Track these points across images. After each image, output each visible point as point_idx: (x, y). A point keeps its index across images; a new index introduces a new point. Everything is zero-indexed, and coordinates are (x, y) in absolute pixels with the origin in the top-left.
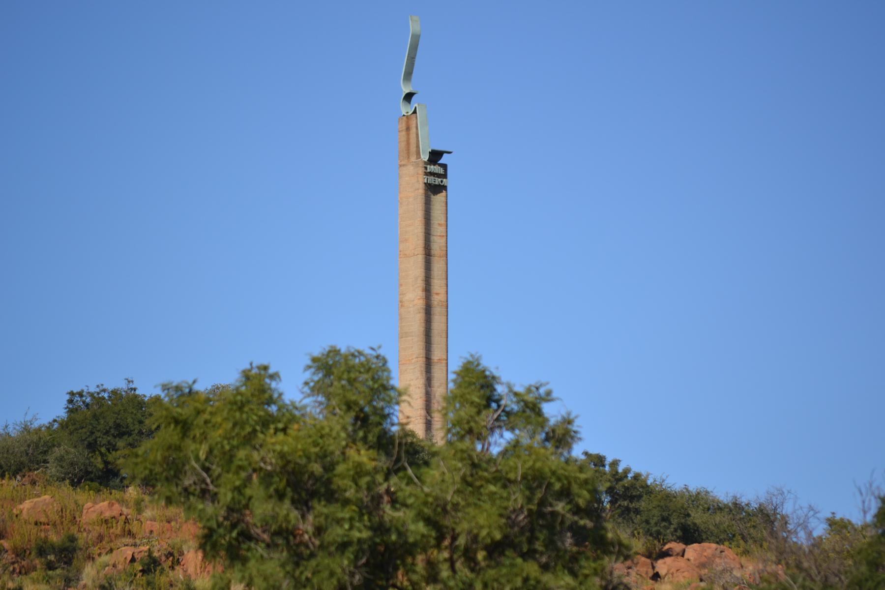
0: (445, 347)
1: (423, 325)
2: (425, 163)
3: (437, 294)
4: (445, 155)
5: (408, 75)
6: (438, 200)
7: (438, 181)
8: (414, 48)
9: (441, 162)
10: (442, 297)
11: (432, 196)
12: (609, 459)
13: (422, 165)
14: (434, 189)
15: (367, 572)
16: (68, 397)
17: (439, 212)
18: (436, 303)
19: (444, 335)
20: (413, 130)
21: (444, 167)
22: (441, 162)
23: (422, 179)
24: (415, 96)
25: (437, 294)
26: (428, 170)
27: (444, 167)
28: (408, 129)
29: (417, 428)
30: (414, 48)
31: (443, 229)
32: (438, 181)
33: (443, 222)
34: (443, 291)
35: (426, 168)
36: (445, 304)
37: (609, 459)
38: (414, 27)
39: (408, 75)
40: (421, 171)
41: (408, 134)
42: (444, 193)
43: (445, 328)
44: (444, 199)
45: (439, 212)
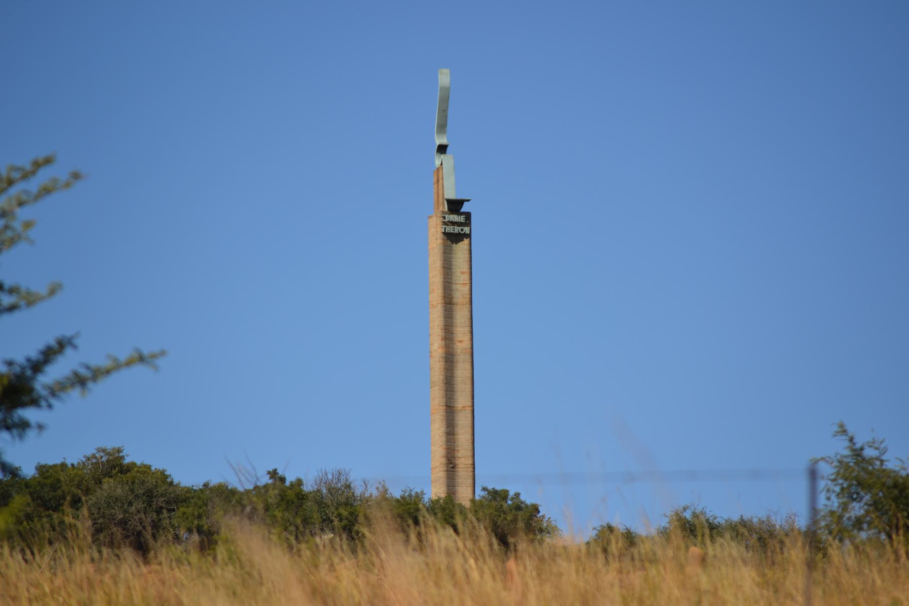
1: (443, 373)
2: (444, 212)
3: (461, 342)
5: (442, 127)
6: (461, 248)
7: (457, 229)
10: (466, 344)
13: (439, 215)
14: (453, 238)
15: (95, 592)
16: (871, 440)
18: (459, 351)
19: (469, 382)
20: (441, 181)
21: (468, 216)
22: (462, 210)
23: (440, 229)
25: (461, 342)
26: (447, 220)
28: (438, 181)
31: (467, 277)
35: (444, 218)
38: (444, 78)
39: (442, 127)
40: (440, 220)
43: (469, 375)
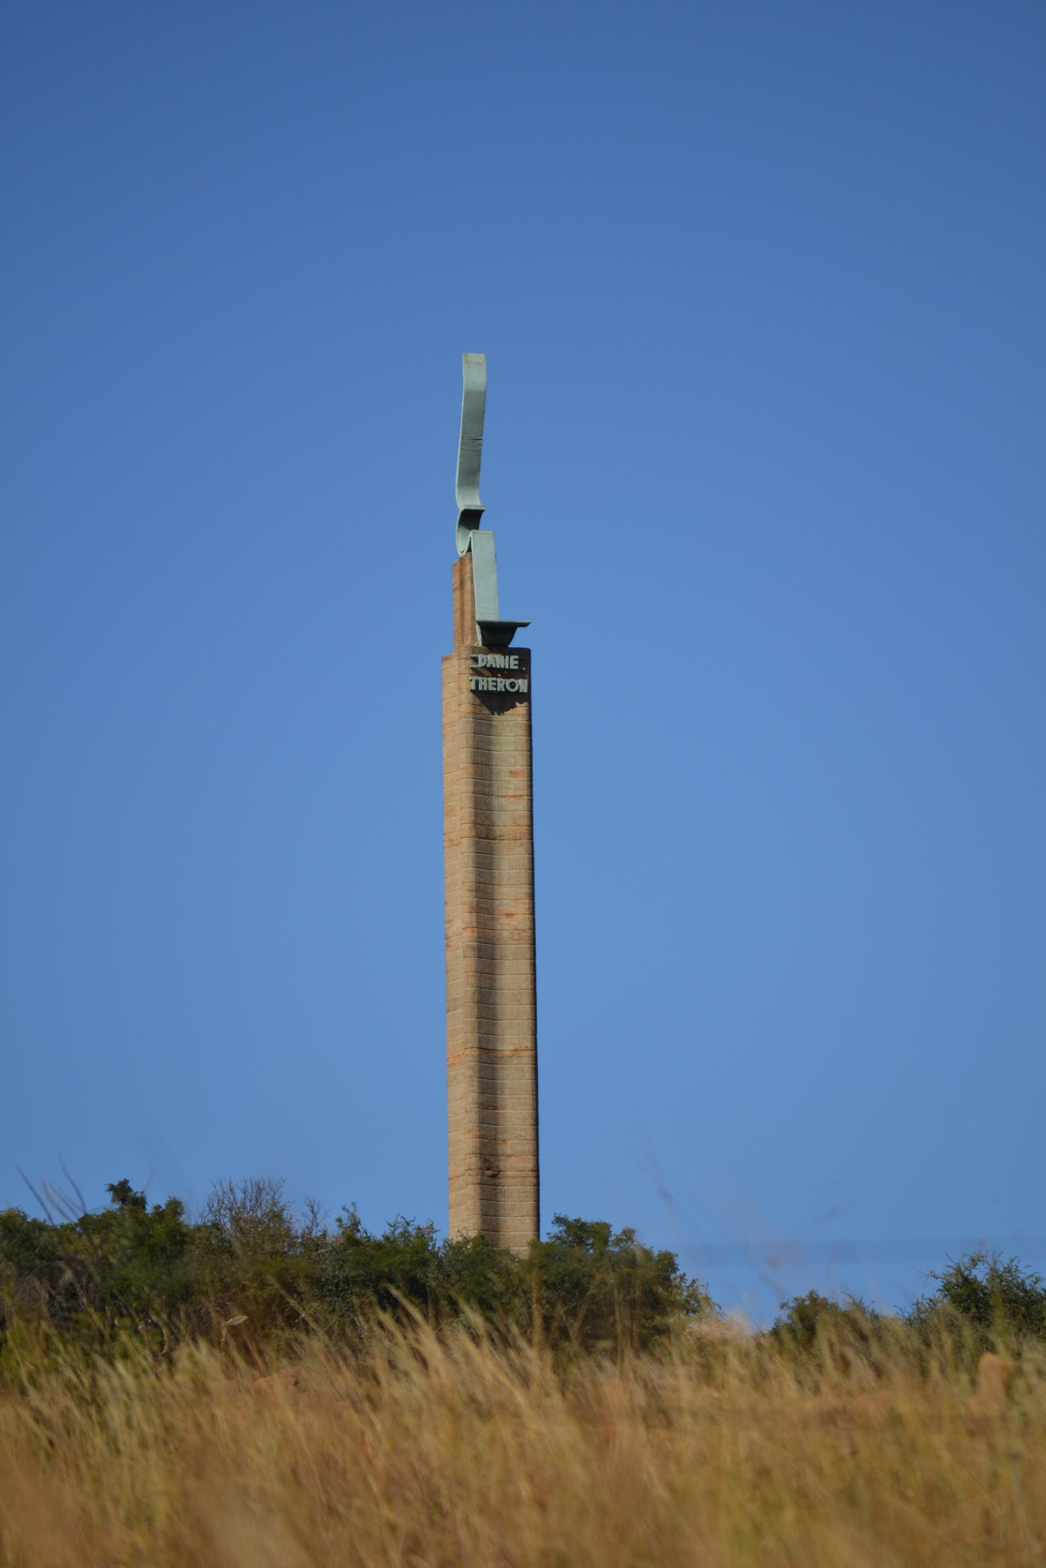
0: (527, 1023)
3: (509, 915)
4: (519, 630)
5: (470, 475)
7: (502, 684)
9: (513, 645)
10: (521, 921)
12: (616, 1231)
14: (492, 702)
17: (511, 747)
18: (506, 934)
19: (526, 999)
21: (524, 656)
23: (467, 683)
25: (509, 915)
26: (481, 664)
29: (65, 1222)
34: (523, 907)
35: (476, 660)
37: (616, 1231)
38: (474, 372)
39: (470, 475)
42: (521, 708)
44: (522, 720)
45: (511, 747)
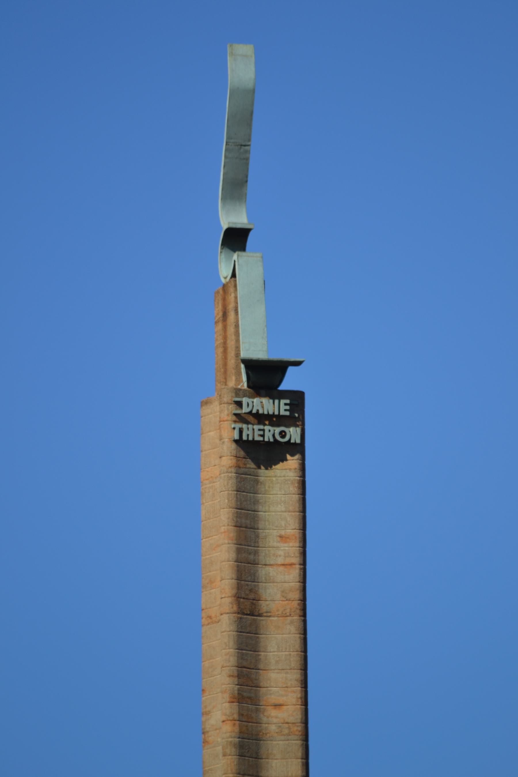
2: (237, 392)
3: (278, 706)
4: (291, 370)
5: (236, 187)
8: (243, 120)
10: (292, 713)
11: (263, 471)
13: (228, 397)
18: (273, 728)
20: (231, 316)
22: (283, 387)
23: (229, 431)
24: (251, 234)
25: (278, 706)
26: (245, 409)
27: (297, 399)
30: (243, 120)
32: (270, 433)
33: (292, 528)
34: (293, 697)
35: (239, 404)
36: (299, 728)
38: (241, 67)
41: (225, 328)
42: (292, 462)
